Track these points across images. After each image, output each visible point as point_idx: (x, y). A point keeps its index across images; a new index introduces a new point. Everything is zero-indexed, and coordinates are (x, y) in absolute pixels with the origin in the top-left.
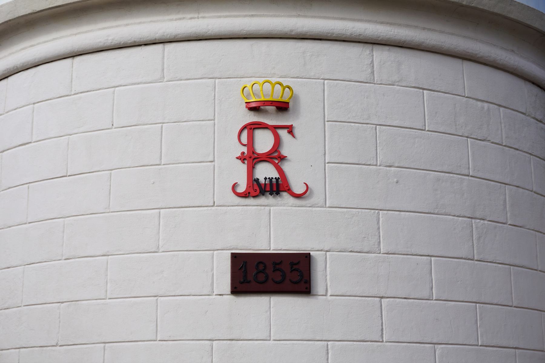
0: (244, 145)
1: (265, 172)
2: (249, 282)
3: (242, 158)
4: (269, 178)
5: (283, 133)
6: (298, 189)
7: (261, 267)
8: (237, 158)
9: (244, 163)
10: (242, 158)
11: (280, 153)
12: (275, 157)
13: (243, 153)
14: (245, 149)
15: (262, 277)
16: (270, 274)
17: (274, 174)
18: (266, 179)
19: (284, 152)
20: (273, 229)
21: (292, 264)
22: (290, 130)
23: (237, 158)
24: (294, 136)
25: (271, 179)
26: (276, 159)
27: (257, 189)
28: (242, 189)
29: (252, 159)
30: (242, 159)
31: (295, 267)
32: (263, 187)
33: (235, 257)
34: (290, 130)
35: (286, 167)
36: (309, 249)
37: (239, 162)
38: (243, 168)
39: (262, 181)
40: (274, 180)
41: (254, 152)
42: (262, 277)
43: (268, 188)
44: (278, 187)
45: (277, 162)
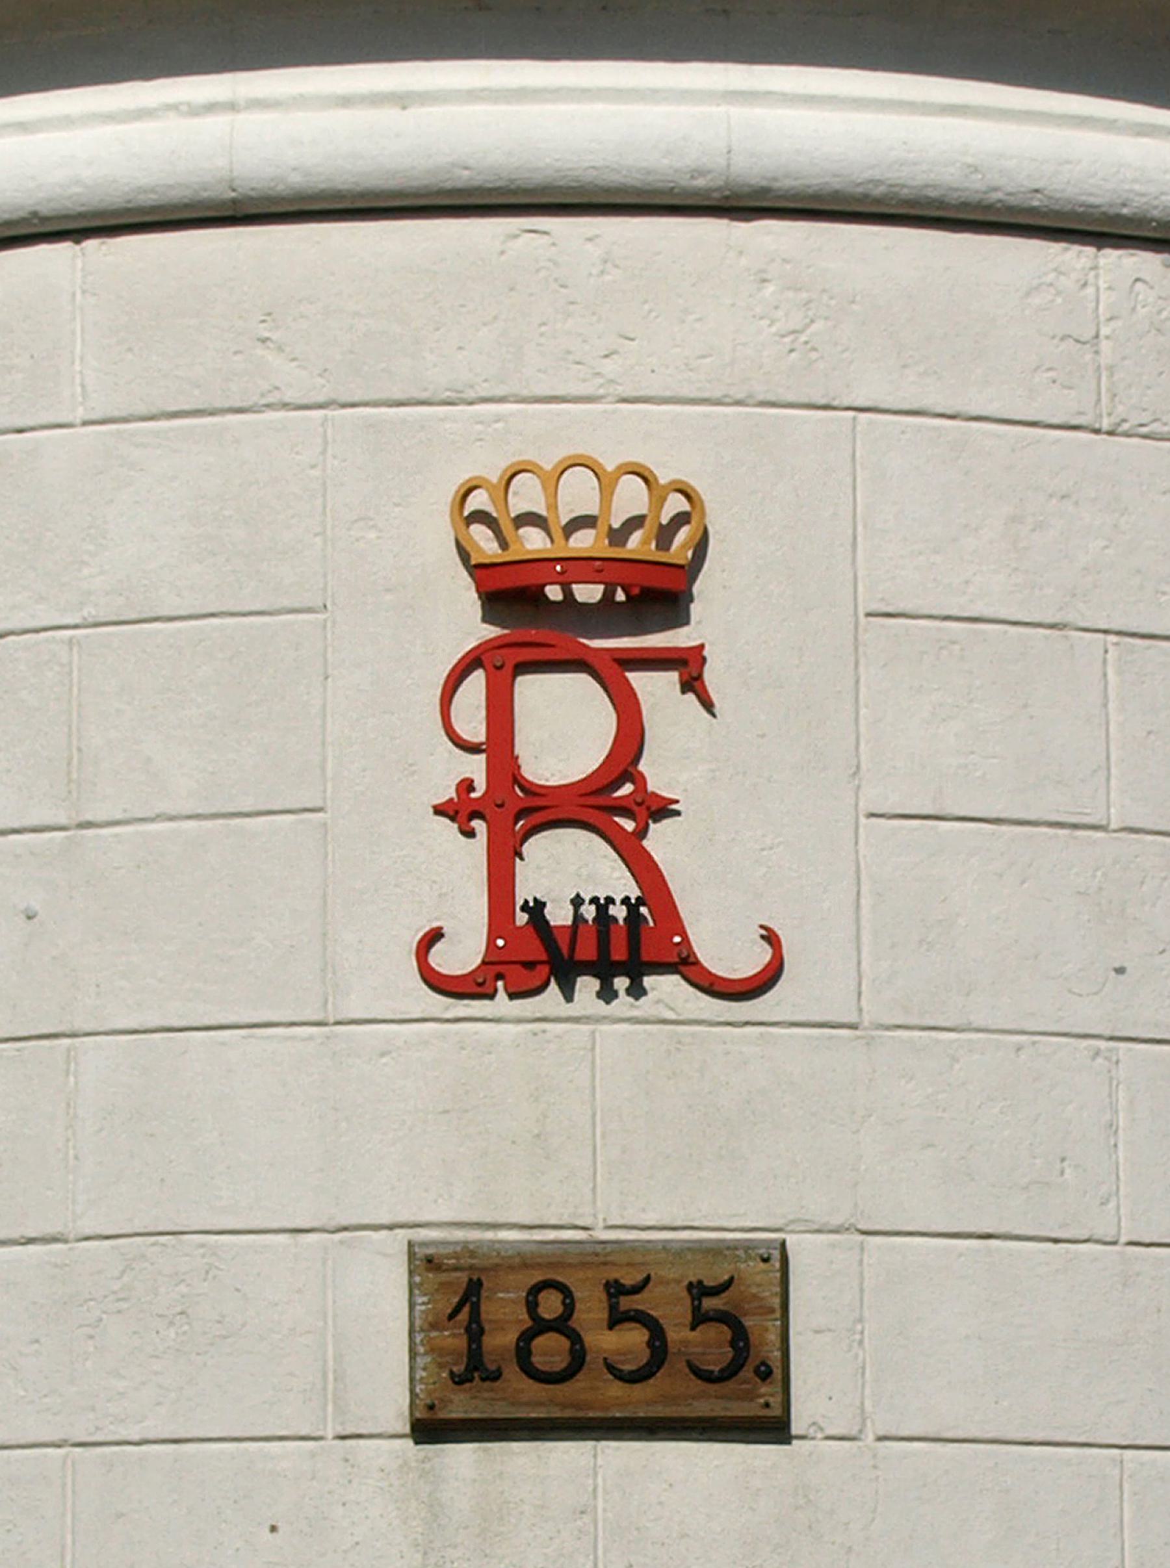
0: (473, 749)
1: (569, 871)
2: (496, 1376)
3: (459, 811)
4: (594, 900)
5: (655, 689)
6: (728, 952)
7: (550, 1305)
8: (439, 811)
9: (470, 834)
10: (459, 811)
11: (639, 781)
12: (616, 802)
13: (467, 786)
14: (476, 768)
15: (550, 1350)
16: (566, 1342)
17: (618, 883)
18: (577, 902)
19: (658, 773)
20: (603, 1134)
21: (615, 1290)
22: (689, 668)
23: (439, 811)
24: (708, 705)
25: (602, 906)
26: (627, 813)
27: (539, 956)
28: (461, 955)
29: (505, 810)
30: (463, 815)
31: (625, 1303)
32: (564, 945)
33: (426, 1264)
34: (689, 668)
35: (661, 841)
36: (779, 1223)
37: (448, 828)
38: (466, 857)
39: (559, 916)
40: (619, 912)
41: (517, 779)
42: (550, 1350)
43: (587, 951)
44: (629, 947)
45: (629, 825)
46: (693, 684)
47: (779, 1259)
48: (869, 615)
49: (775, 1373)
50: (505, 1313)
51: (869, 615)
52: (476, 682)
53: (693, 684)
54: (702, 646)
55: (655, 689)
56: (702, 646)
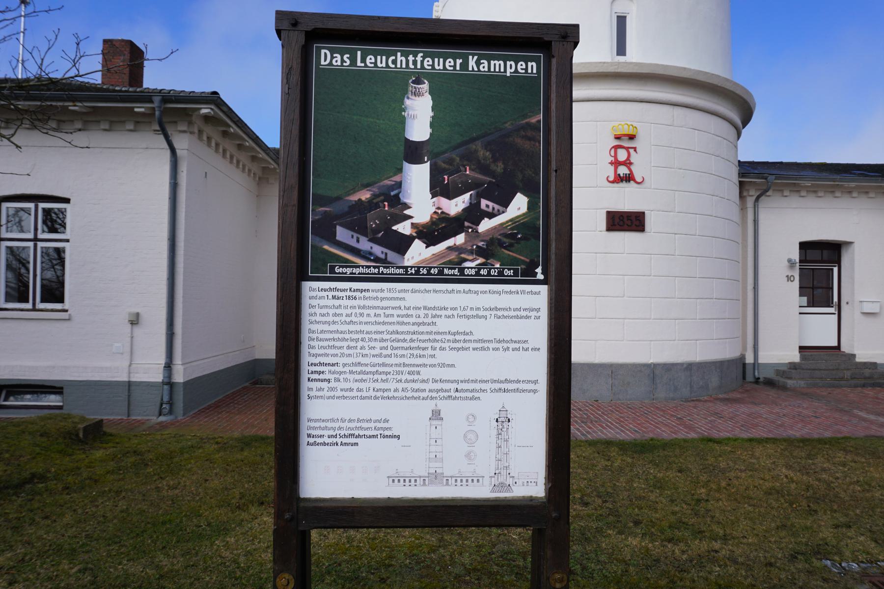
1: (623, 170)
3: (611, 163)
6: (639, 179)
10: (611, 163)
12: (628, 163)
14: (613, 159)
22: (635, 149)
27: (619, 179)
28: (611, 179)
29: (616, 163)
35: (632, 168)
38: (612, 168)
44: (629, 178)
46: (635, 151)
47: (644, 213)
48: (621, 49)
49: (643, 226)
50: (617, 220)
51: (621, 49)
52: (613, 150)
53: (635, 151)
54: (427, 247)
55: (631, 151)
56: (427, 247)
